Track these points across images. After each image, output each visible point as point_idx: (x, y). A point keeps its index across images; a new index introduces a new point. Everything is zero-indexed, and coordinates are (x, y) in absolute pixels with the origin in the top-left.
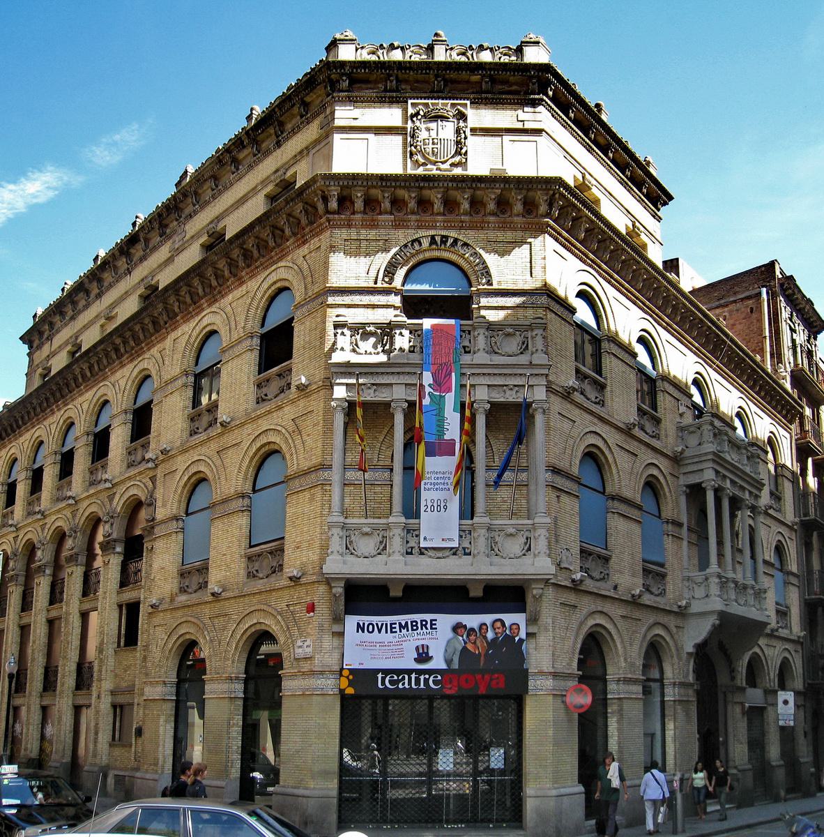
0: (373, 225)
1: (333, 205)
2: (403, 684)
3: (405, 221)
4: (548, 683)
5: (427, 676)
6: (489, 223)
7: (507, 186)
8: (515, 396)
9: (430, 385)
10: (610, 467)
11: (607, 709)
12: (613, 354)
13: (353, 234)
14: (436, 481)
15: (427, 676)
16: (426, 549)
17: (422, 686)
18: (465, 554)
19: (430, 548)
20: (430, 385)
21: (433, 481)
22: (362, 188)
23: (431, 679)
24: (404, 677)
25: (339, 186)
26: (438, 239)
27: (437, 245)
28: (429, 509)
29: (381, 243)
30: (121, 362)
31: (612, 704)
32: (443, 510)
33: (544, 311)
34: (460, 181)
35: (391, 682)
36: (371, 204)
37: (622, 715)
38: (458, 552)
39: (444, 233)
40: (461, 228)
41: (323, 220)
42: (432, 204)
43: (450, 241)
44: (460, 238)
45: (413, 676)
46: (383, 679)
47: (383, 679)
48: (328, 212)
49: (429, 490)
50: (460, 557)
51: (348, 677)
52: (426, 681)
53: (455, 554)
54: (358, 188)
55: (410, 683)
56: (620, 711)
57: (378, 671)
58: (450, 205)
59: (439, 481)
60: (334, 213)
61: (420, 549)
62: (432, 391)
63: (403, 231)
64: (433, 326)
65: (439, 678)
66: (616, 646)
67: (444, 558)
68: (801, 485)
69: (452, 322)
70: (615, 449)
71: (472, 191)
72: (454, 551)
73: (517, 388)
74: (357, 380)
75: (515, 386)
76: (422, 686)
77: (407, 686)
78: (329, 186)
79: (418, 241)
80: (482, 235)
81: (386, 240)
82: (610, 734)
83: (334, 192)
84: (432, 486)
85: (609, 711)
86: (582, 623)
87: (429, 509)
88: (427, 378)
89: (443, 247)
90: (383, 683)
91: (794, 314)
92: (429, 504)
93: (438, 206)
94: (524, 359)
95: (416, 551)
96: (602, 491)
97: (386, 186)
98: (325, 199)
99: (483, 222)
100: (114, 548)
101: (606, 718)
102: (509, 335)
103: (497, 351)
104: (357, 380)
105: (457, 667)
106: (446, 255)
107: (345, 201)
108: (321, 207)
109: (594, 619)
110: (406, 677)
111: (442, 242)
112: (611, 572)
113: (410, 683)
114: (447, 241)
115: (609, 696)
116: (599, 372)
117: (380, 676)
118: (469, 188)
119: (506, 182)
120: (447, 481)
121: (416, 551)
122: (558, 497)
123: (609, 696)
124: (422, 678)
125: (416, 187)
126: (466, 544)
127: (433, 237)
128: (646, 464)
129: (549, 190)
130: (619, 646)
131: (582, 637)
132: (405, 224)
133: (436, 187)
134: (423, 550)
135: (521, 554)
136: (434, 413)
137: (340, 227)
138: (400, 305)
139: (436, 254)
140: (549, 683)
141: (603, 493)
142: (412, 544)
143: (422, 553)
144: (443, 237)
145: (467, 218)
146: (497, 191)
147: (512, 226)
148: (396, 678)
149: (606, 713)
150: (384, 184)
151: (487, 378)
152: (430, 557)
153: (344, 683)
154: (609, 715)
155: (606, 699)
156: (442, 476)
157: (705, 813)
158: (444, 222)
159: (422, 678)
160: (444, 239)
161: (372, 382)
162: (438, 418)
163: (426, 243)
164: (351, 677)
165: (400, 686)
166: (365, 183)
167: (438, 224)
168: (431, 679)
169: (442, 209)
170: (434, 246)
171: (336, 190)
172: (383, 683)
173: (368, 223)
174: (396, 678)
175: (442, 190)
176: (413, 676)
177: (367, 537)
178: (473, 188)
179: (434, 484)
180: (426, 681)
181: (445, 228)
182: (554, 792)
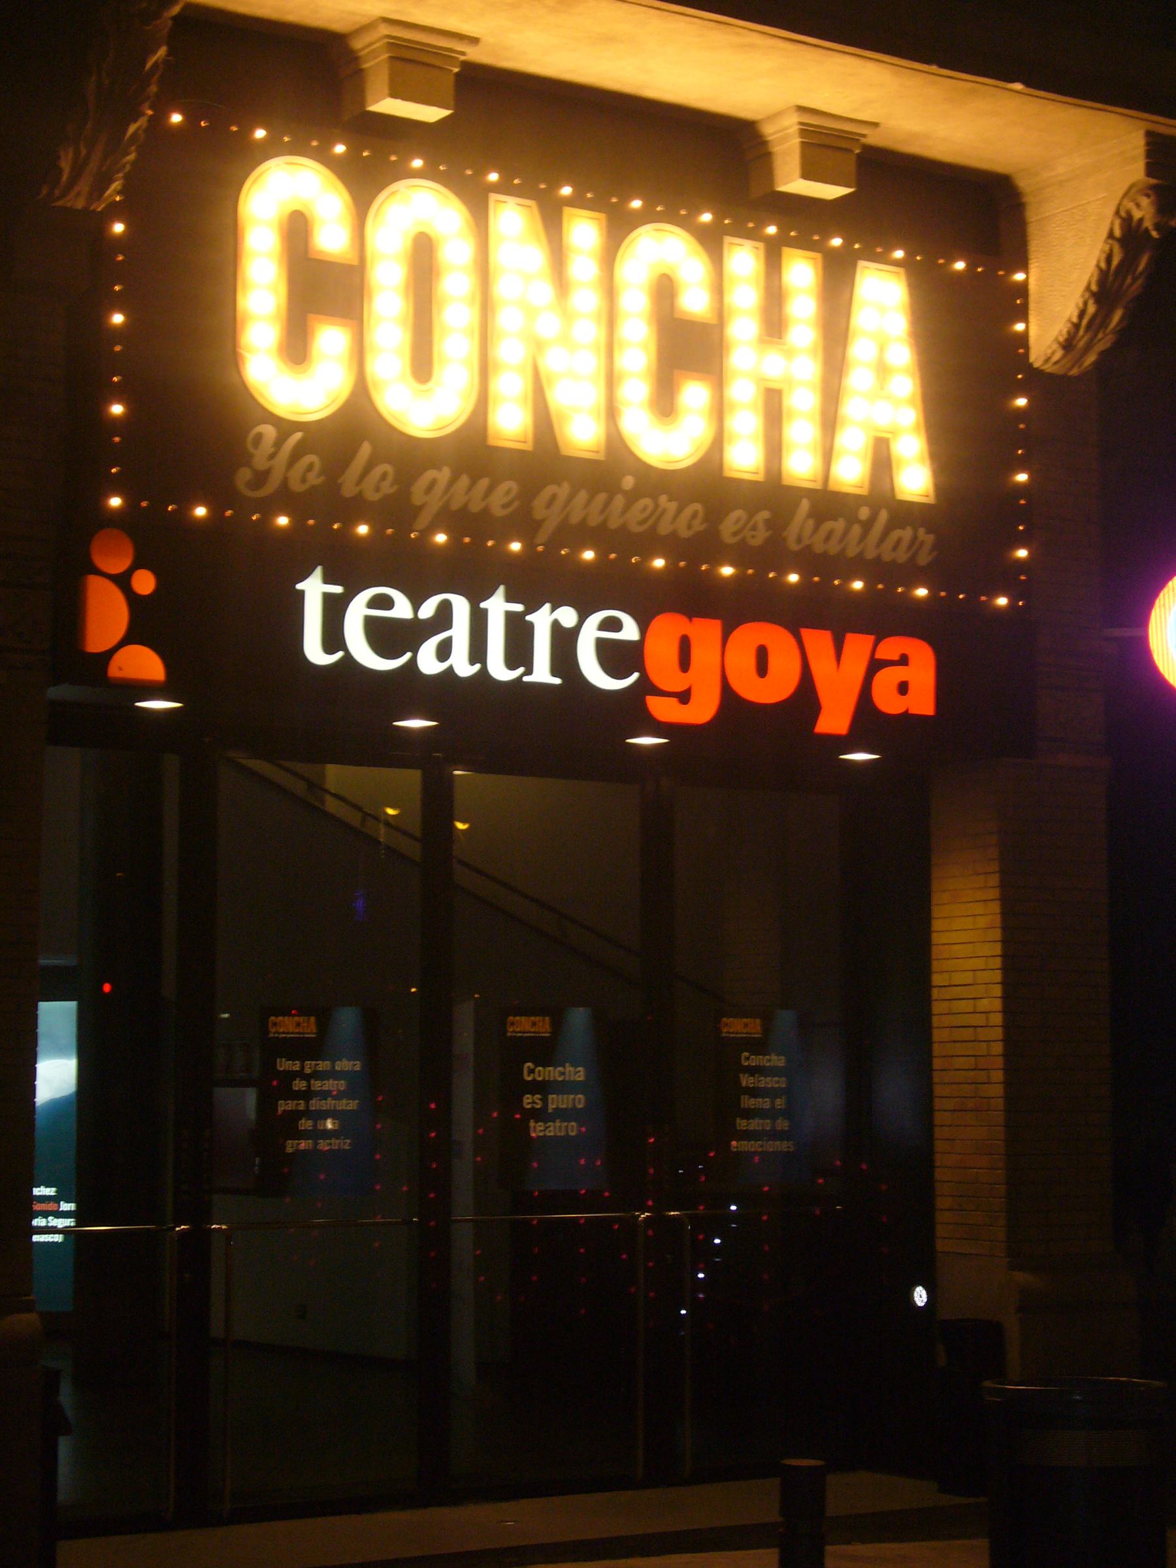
2: (444, 651)
24: (445, 611)
35: (385, 636)
46: (334, 610)
47: (334, 610)
51: (123, 581)
52: (564, 641)
55: (478, 652)
68: (794, 1462)
74: (309, 1086)
90: (333, 638)
91: (288, 764)
104: (309, 1086)
105: (54, 1189)
113: (478, 652)
138: (418, 834)
148: (402, 609)
159: (542, 620)
164: (145, 583)
172: (333, 638)
180: (564, 641)
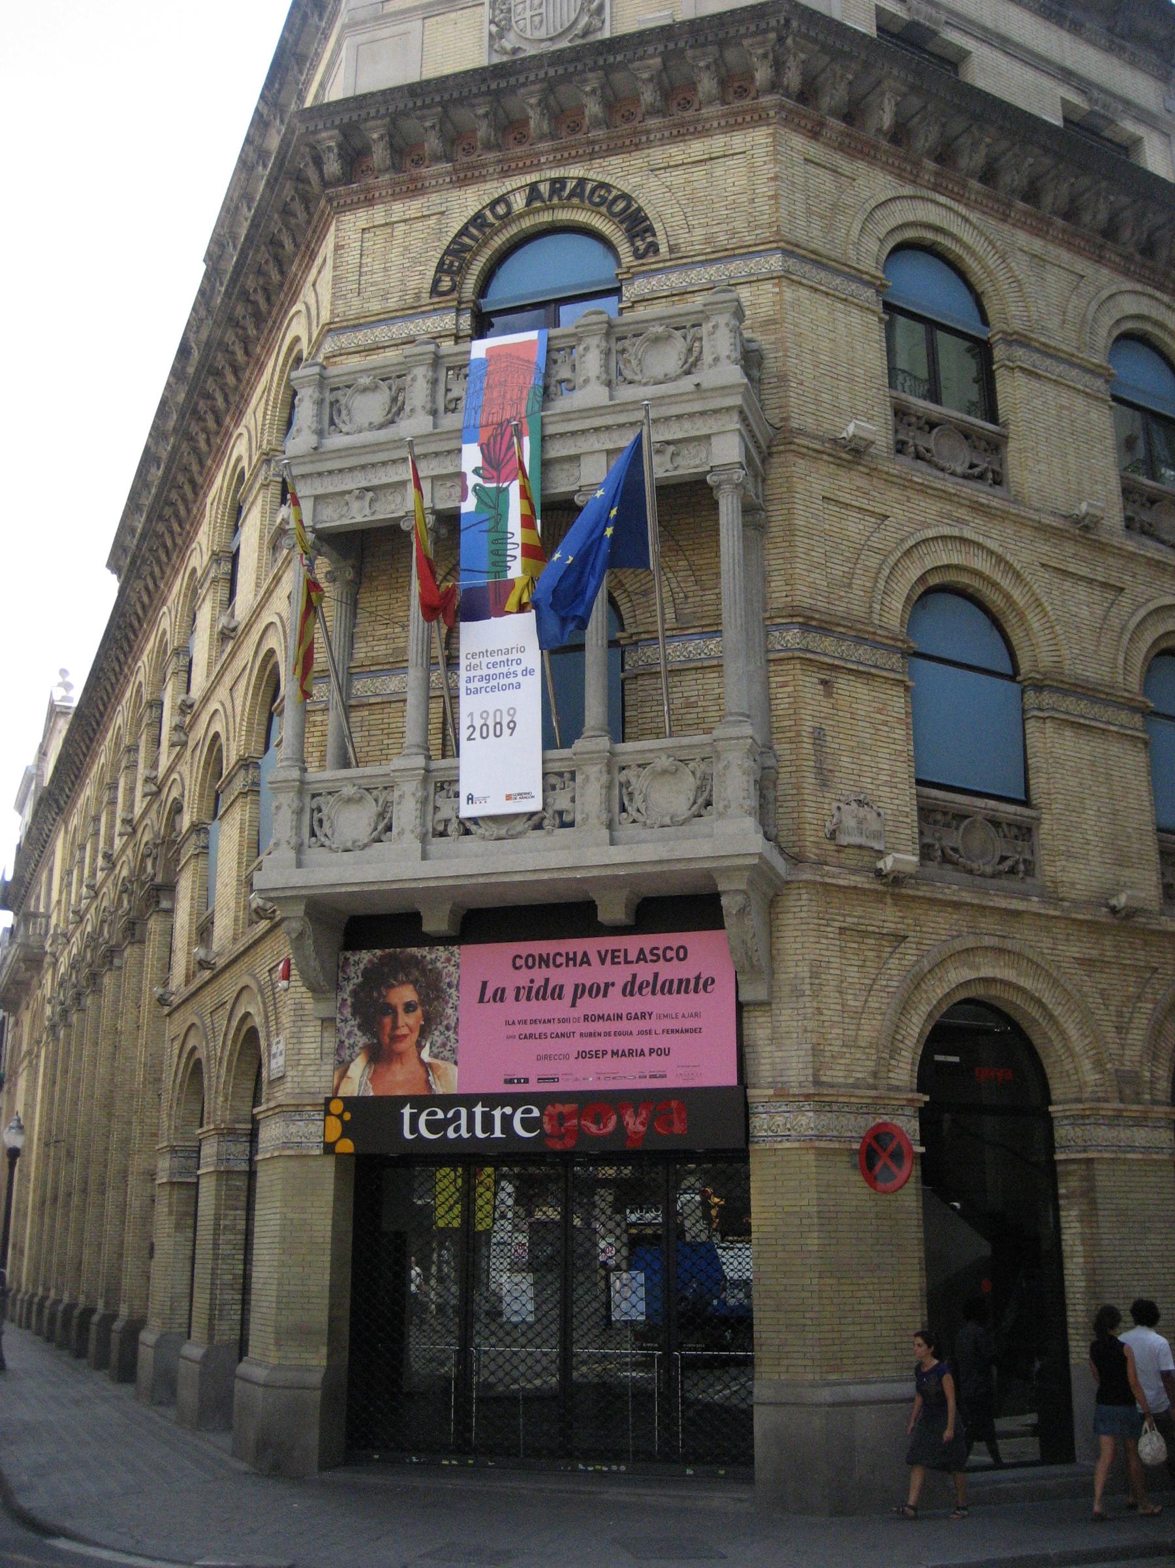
0: (415, 189)
1: (333, 167)
2: (457, 1129)
3: (474, 168)
4: (803, 1120)
5: (508, 1110)
6: (648, 132)
7: (671, 46)
8: (670, 466)
9: (476, 471)
10: (1021, 615)
11: (1055, 1188)
12: (1022, 369)
13: (378, 214)
14: (492, 671)
15: (508, 1110)
16: (475, 820)
17: (498, 1133)
18: (564, 825)
19: (484, 818)
20: (476, 471)
21: (485, 672)
22: (379, 122)
23: (518, 1115)
25: (333, 127)
26: (544, 188)
27: (544, 201)
28: (477, 734)
29: (432, 221)
30: (174, 567)
31: (1069, 1173)
32: (507, 731)
33: (775, 285)
34: (572, 61)
35: (432, 1126)
36: (404, 153)
37: (1093, 1203)
38: (546, 822)
39: (555, 174)
40: (592, 156)
41: (323, 203)
42: (525, 122)
43: (570, 185)
44: (591, 175)
45: (478, 1110)
46: (414, 1119)
47: (414, 1119)
48: (326, 184)
49: (477, 691)
50: (550, 833)
51: (340, 1116)
52: (507, 1120)
53: (539, 827)
54: (371, 123)
56: (1089, 1193)
57: (402, 1101)
58: (564, 120)
59: (498, 671)
60: (337, 182)
61: (461, 822)
62: (480, 481)
63: (475, 188)
64: (489, 350)
65: (536, 1113)
66: (1062, 1033)
67: (512, 837)
69: (533, 335)
70: (1040, 582)
71: (600, 73)
72: (535, 821)
73: (672, 448)
75: (668, 443)
76: (498, 1133)
77: (465, 1134)
78: (316, 132)
79: (502, 199)
80: (637, 160)
81: (442, 213)
82: (1066, 1248)
83: (329, 139)
84: (483, 684)
85: (1062, 1191)
86: (918, 982)
87: (477, 734)
88: (472, 457)
89: (555, 201)
90: (414, 1128)
92: (478, 723)
93: (536, 122)
94: (687, 384)
95: (453, 827)
96: (1007, 669)
97: (423, 107)
98: (318, 162)
99: (635, 133)
100: (158, 903)
101: (1057, 1209)
102: (657, 340)
103: (630, 376)
106: (563, 216)
107: (354, 159)
108: (312, 174)
109: (974, 967)
110: (464, 1111)
111: (553, 192)
112: (1043, 856)
114: (563, 187)
115: (1059, 1156)
116: (992, 415)
117: (407, 1111)
118: (591, 70)
119: (668, 39)
120: (514, 668)
121: (453, 827)
122: (824, 682)
123: (1059, 1156)
124: (497, 1113)
125: (483, 94)
126: (561, 801)
127: (533, 187)
128: (1151, 606)
129: (766, 31)
130: (1073, 1032)
131: (924, 1009)
132: (477, 174)
133: (524, 85)
134: (468, 824)
135: (688, 814)
136: (486, 526)
137: (352, 206)
139: (546, 217)
140: (807, 1120)
141: (1013, 677)
142: (445, 813)
143: (467, 832)
144: (554, 181)
145: (599, 133)
146: (651, 62)
147: (700, 128)
148: (440, 1115)
149: (1056, 1197)
150: (419, 103)
151: (604, 436)
152: (483, 838)
153: (334, 1128)
154: (1061, 1202)
155: (1053, 1163)
156: (504, 658)
157: (912, 1461)
158: (556, 150)
159: (497, 1113)
160: (558, 184)
161: (364, 484)
162: (494, 536)
163: (519, 202)
165: (451, 1134)
166: (383, 111)
167: (543, 160)
168: (518, 1115)
169: (545, 127)
170: (538, 204)
171: (331, 138)
172: (414, 1128)
173: (404, 189)
174: (440, 1115)
175: (537, 87)
176: (478, 1110)
177: (353, 808)
178: (601, 68)
179: (487, 678)
180: (507, 1120)
181: (560, 163)
182: (825, 1395)
